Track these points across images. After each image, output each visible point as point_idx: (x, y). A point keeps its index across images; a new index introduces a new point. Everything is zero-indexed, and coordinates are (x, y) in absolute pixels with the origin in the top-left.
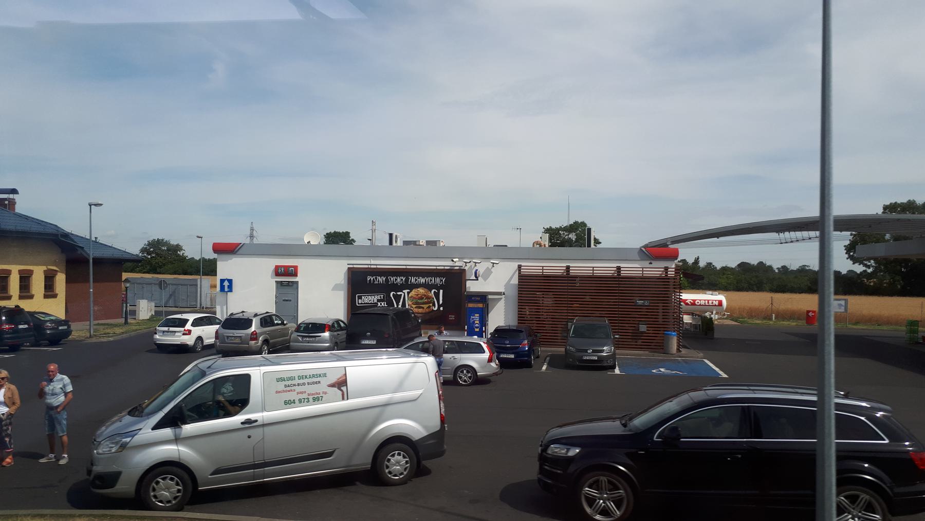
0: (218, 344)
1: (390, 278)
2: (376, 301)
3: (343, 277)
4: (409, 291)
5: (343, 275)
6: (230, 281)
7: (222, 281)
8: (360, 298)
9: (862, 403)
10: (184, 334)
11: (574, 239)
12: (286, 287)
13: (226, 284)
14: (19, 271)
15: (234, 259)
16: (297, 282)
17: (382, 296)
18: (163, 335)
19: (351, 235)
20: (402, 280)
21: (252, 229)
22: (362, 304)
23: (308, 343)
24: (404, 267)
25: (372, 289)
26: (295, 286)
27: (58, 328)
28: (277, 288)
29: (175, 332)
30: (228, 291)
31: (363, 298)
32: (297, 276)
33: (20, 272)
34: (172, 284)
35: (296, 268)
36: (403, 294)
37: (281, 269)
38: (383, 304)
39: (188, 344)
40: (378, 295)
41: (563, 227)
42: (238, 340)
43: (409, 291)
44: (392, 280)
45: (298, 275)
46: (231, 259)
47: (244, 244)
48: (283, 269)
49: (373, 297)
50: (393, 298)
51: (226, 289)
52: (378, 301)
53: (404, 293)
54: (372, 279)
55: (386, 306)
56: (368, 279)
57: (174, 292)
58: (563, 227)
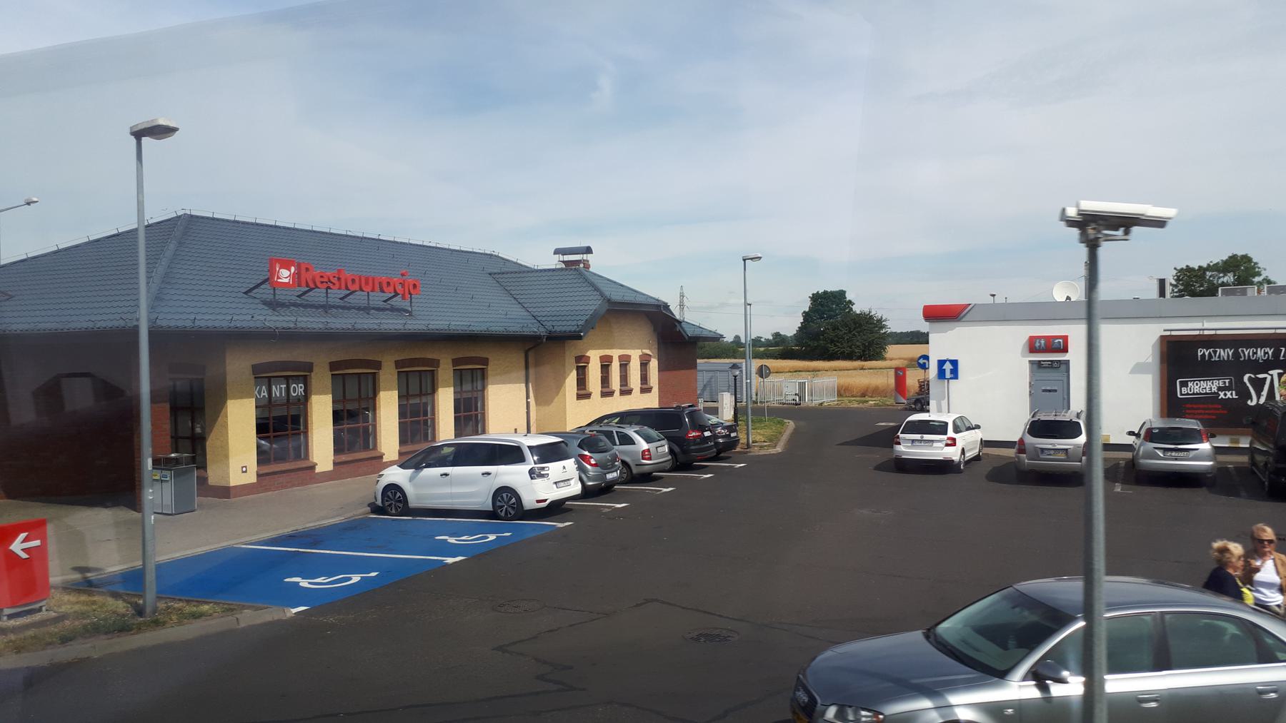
0: (1026, 461)
1: (1243, 351)
2: (1215, 389)
3: (1151, 352)
4: (1281, 371)
5: (1151, 348)
6: (954, 363)
7: (941, 363)
8: (1184, 384)
9: (1095, 515)
10: (947, 445)
11: (1254, 280)
12: (1048, 370)
13: (948, 367)
14: (601, 357)
15: (957, 328)
16: (1067, 363)
17: (1227, 381)
18: (913, 446)
19: (847, 295)
20: (1267, 353)
21: (682, 296)
22: (1188, 394)
23: (1176, 459)
24: (1273, 331)
25: (1209, 369)
26: (1063, 367)
27: (730, 435)
28: (1032, 371)
29: (932, 441)
30: (951, 378)
31: (1190, 384)
32: (1067, 351)
33: (621, 357)
34: (707, 371)
35: (1065, 338)
36: (1269, 378)
37: (1040, 343)
38: (1229, 394)
39: (953, 460)
40: (1219, 380)
41: (1211, 264)
42: (1062, 456)
43: (1281, 371)
44: (1246, 353)
45: (1069, 350)
46: (952, 329)
47: (975, 304)
48: (1043, 342)
49: (1209, 383)
50: (1248, 385)
51: (948, 375)
52: (1220, 389)
53: (1272, 375)
54: (1207, 354)
55: (1234, 397)
56: (1199, 354)
57: (709, 381)
58: (1211, 264)
